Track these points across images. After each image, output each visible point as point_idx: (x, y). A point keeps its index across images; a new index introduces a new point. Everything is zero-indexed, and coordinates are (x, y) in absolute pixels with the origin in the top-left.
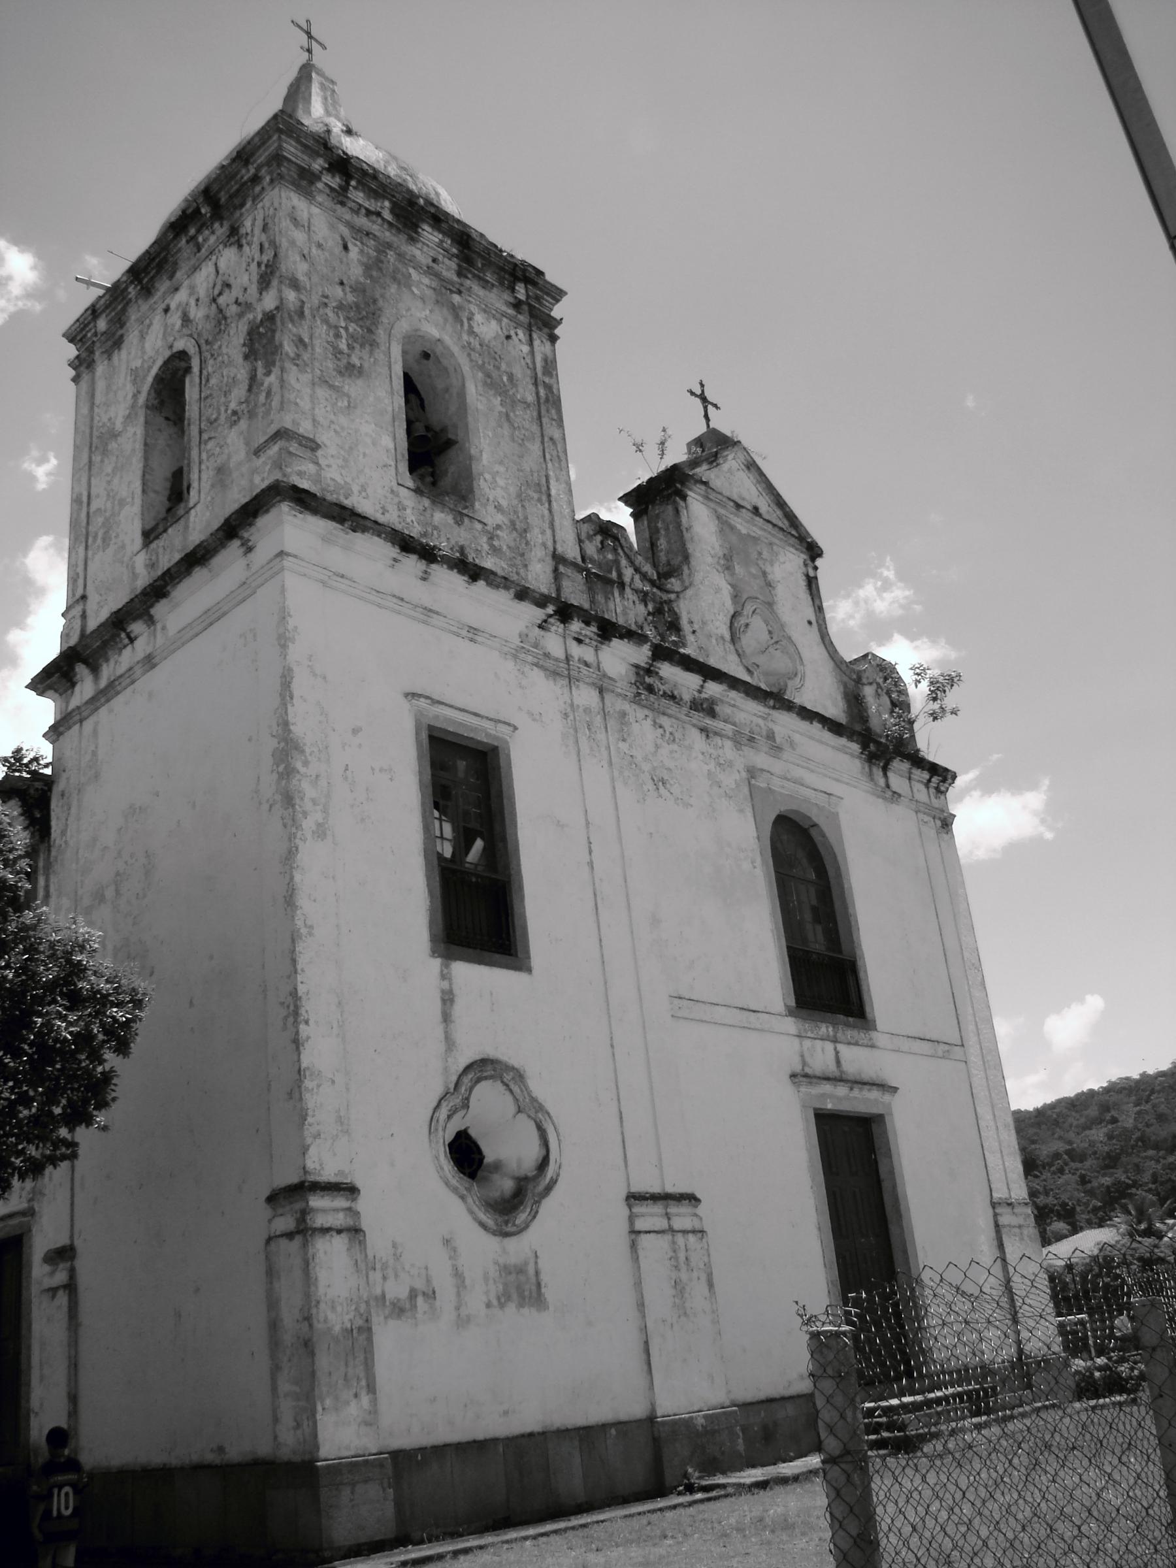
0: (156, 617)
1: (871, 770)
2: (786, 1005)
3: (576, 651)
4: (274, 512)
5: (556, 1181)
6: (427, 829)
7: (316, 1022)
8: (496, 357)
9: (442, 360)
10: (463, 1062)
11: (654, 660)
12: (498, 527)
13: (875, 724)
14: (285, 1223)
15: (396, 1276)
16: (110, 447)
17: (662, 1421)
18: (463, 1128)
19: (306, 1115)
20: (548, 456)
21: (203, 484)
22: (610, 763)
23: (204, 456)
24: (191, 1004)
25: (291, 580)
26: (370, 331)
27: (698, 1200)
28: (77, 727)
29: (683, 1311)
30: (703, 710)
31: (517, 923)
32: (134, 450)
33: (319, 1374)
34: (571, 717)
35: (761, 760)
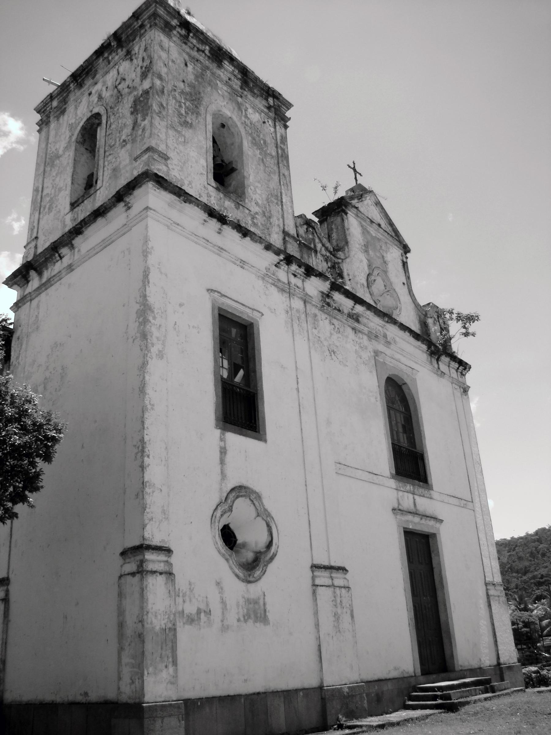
0: (75, 245)
1: (431, 360)
2: (390, 473)
3: (293, 280)
4: (144, 187)
5: (276, 555)
6: (216, 361)
7: (153, 457)
8: (258, 131)
9: (231, 128)
10: (230, 486)
11: (331, 290)
12: (257, 213)
13: (433, 338)
14: (131, 567)
15: (190, 601)
16: (55, 163)
17: (327, 689)
18: (227, 523)
19: (146, 507)
20: (282, 183)
21: (105, 177)
22: (309, 339)
23: (106, 163)
24: (83, 447)
25: (151, 222)
26: (196, 107)
27: (347, 571)
28: (29, 303)
29: (338, 630)
30: (353, 319)
31: (260, 415)
32: (68, 163)
33: (146, 653)
34: (290, 313)
35: (381, 347)
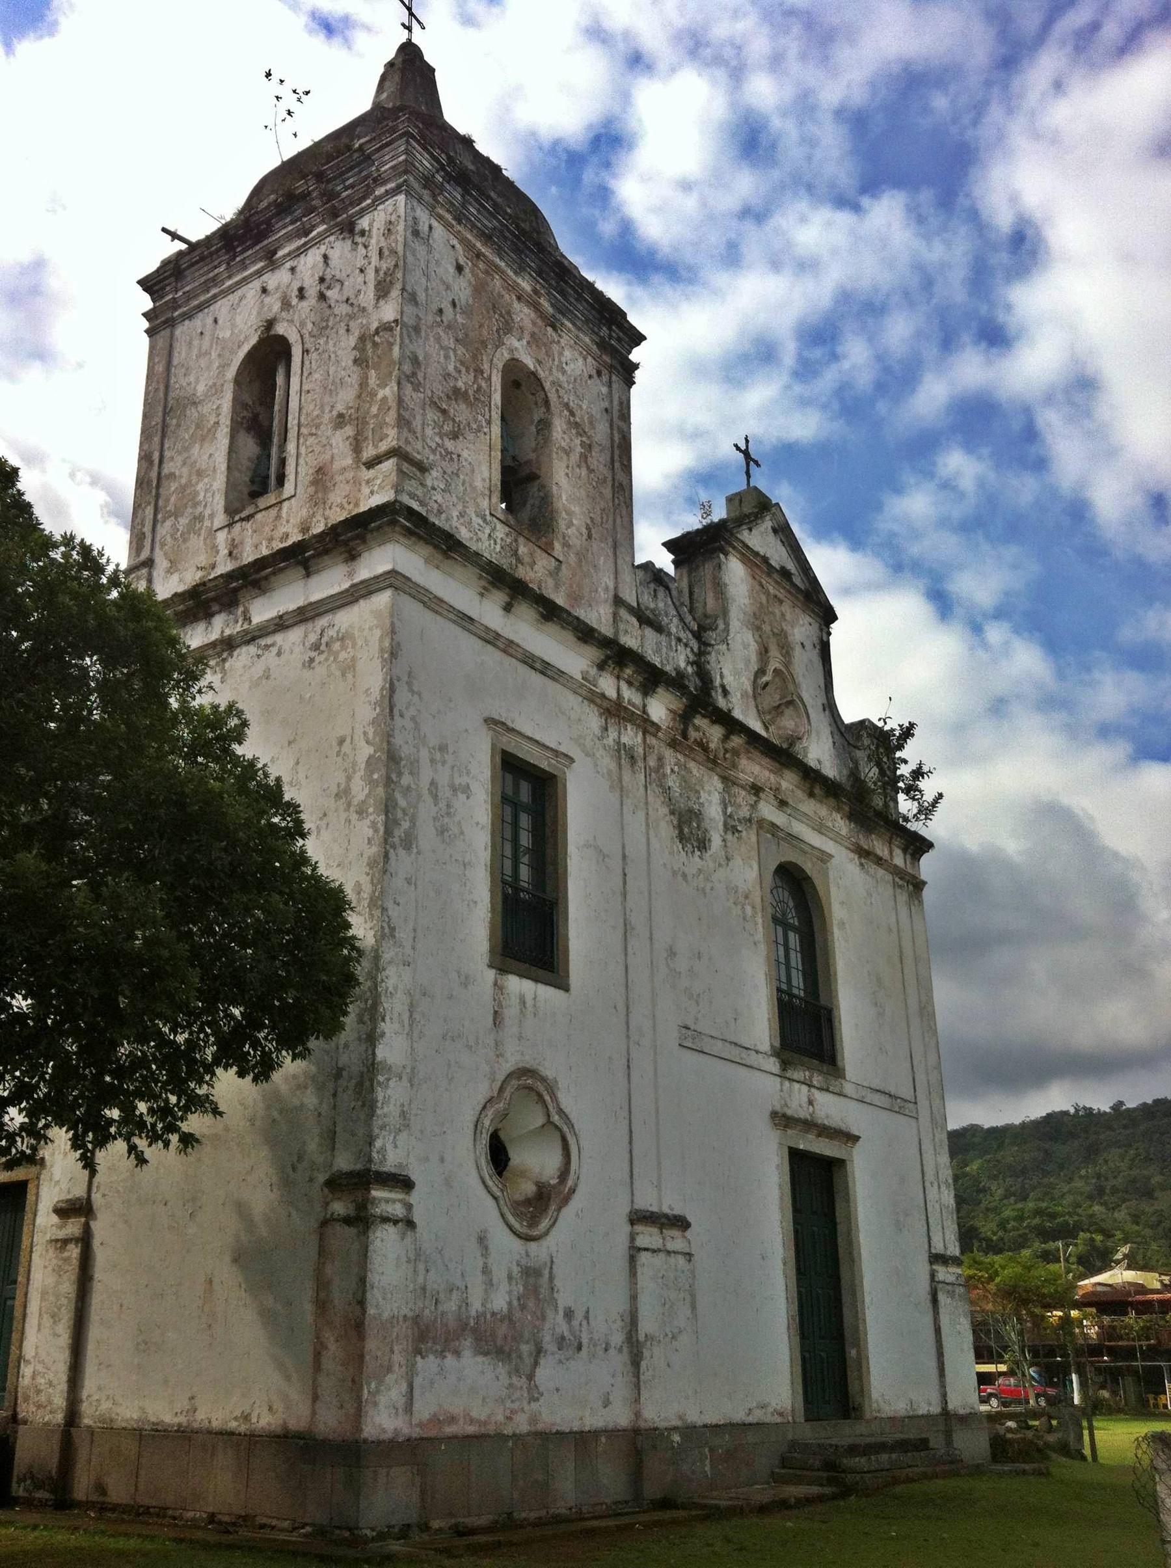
2: (772, 1046)
5: (574, 1191)
10: (508, 1066)
14: (339, 1208)
23: (303, 450)
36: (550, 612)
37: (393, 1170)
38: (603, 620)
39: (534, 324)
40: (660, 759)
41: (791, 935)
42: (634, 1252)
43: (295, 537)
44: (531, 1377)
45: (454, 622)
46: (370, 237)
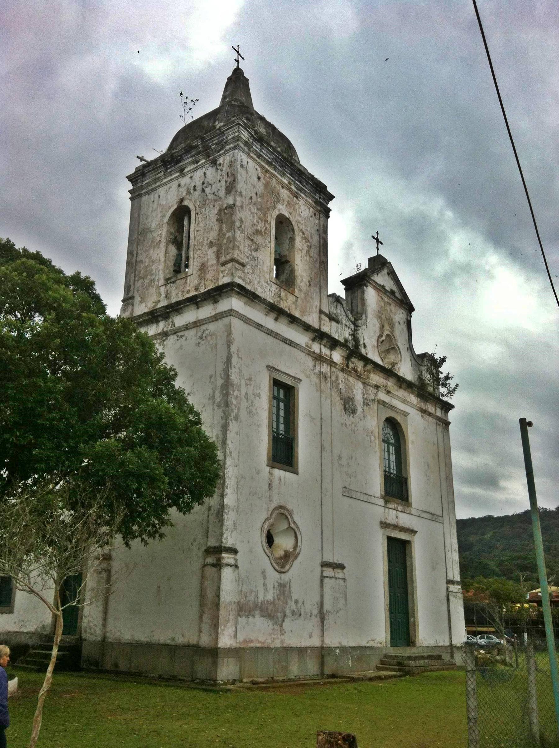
10: (274, 505)
36: (293, 320)
37: (230, 546)
38: (315, 320)
39: (289, 197)
40: (337, 377)
41: (391, 447)
42: (323, 578)
43: (193, 293)
44: (281, 626)
45: (255, 327)
46: (223, 166)
